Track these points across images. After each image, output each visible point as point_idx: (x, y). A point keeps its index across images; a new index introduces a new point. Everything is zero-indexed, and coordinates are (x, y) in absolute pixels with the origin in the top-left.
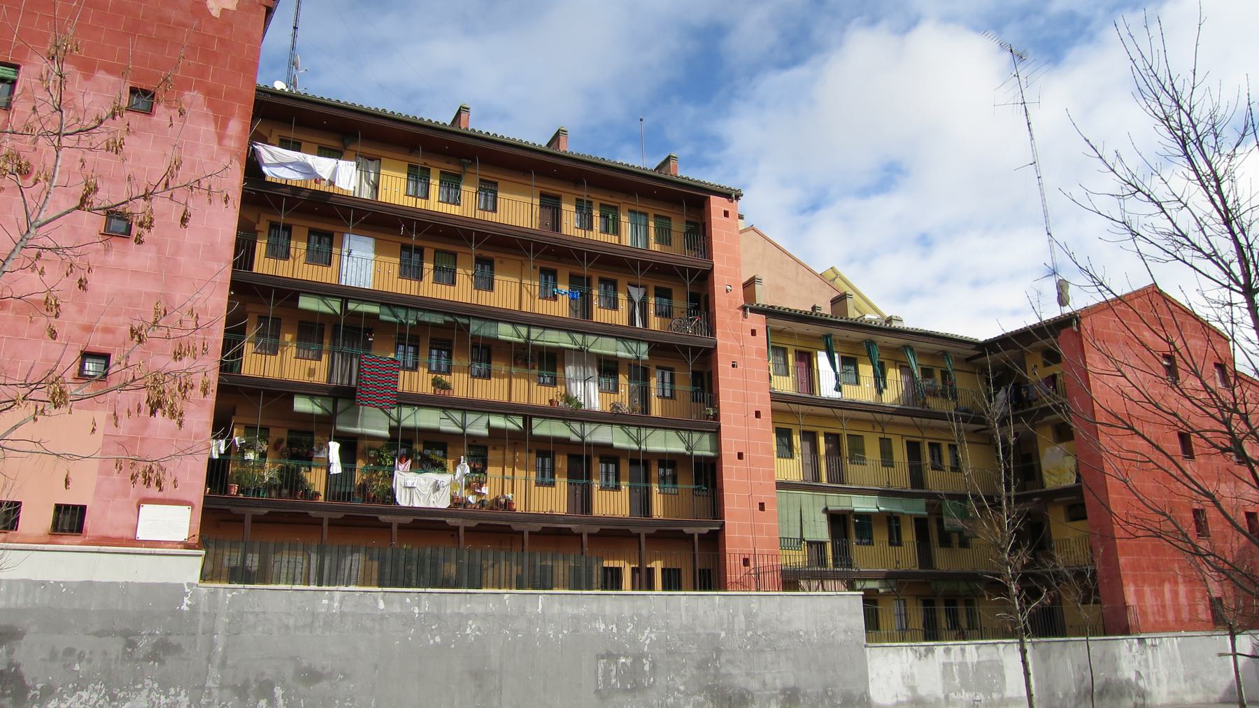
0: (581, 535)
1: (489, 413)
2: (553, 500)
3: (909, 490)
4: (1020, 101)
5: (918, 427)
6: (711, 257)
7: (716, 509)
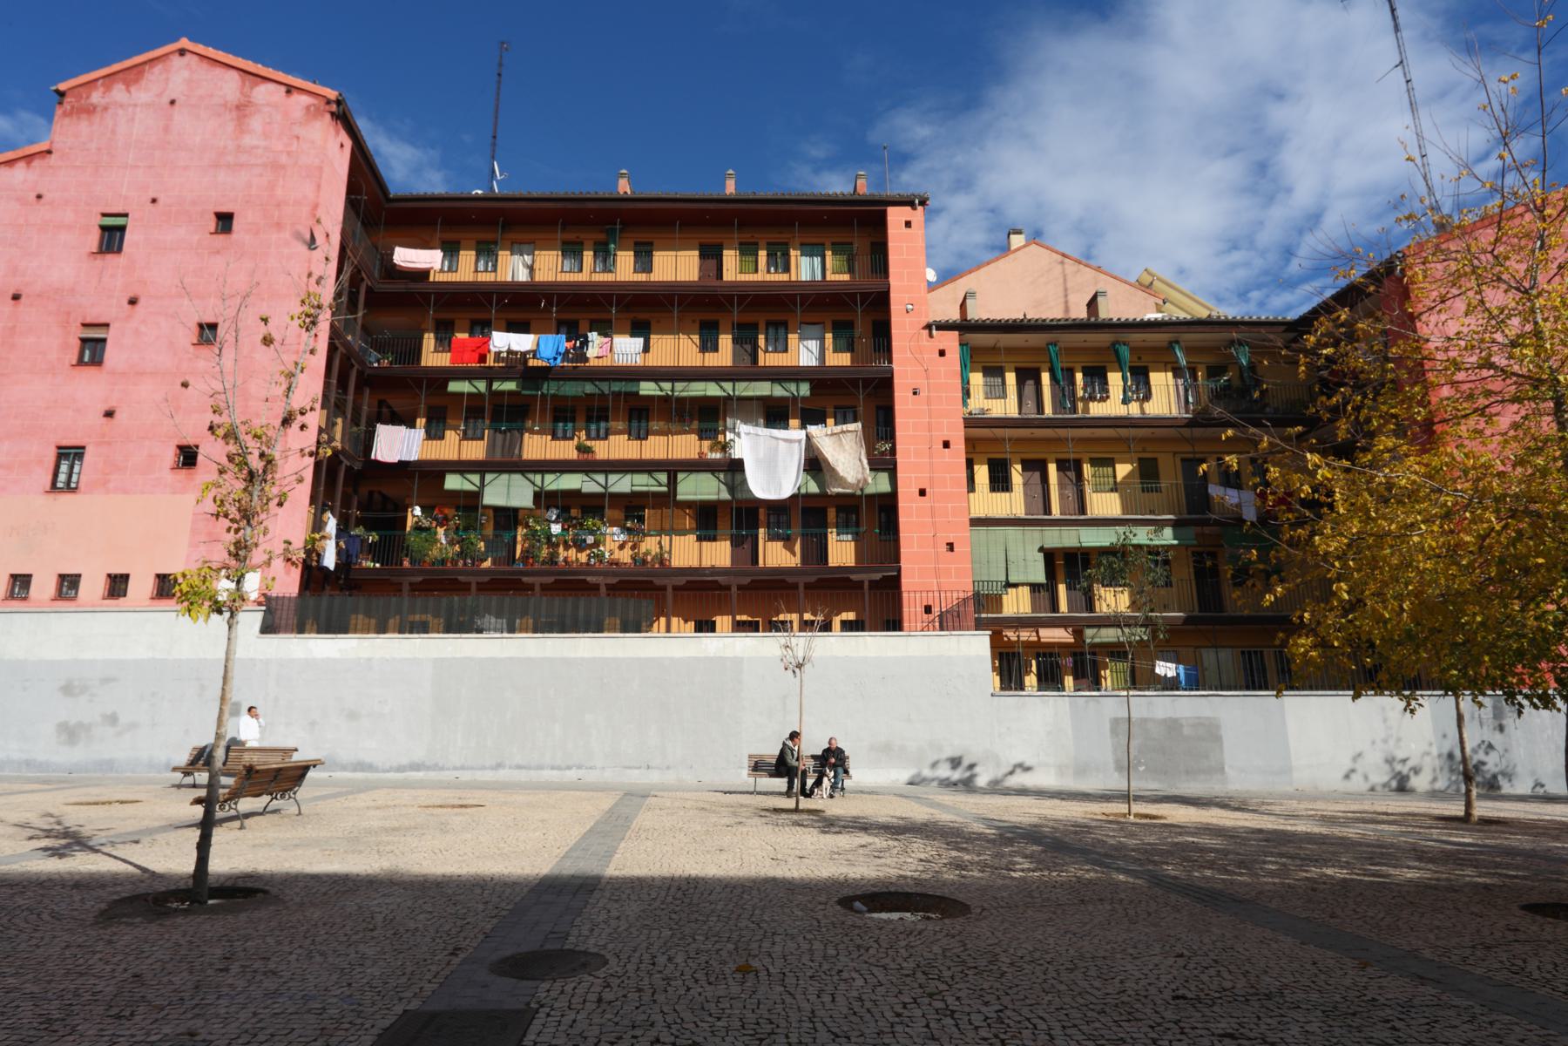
0: (728, 588)
1: (633, 472)
2: (719, 554)
3: (1023, 516)
5: (1186, 440)
6: (887, 276)
7: (892, 553)
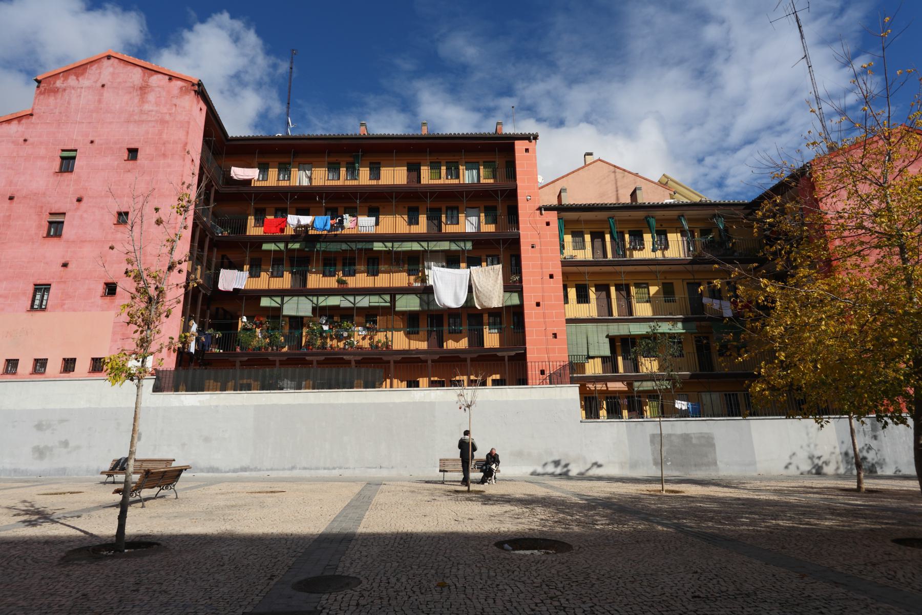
0: (426, 361)
4: (790, 11)
6: (515, 180)
